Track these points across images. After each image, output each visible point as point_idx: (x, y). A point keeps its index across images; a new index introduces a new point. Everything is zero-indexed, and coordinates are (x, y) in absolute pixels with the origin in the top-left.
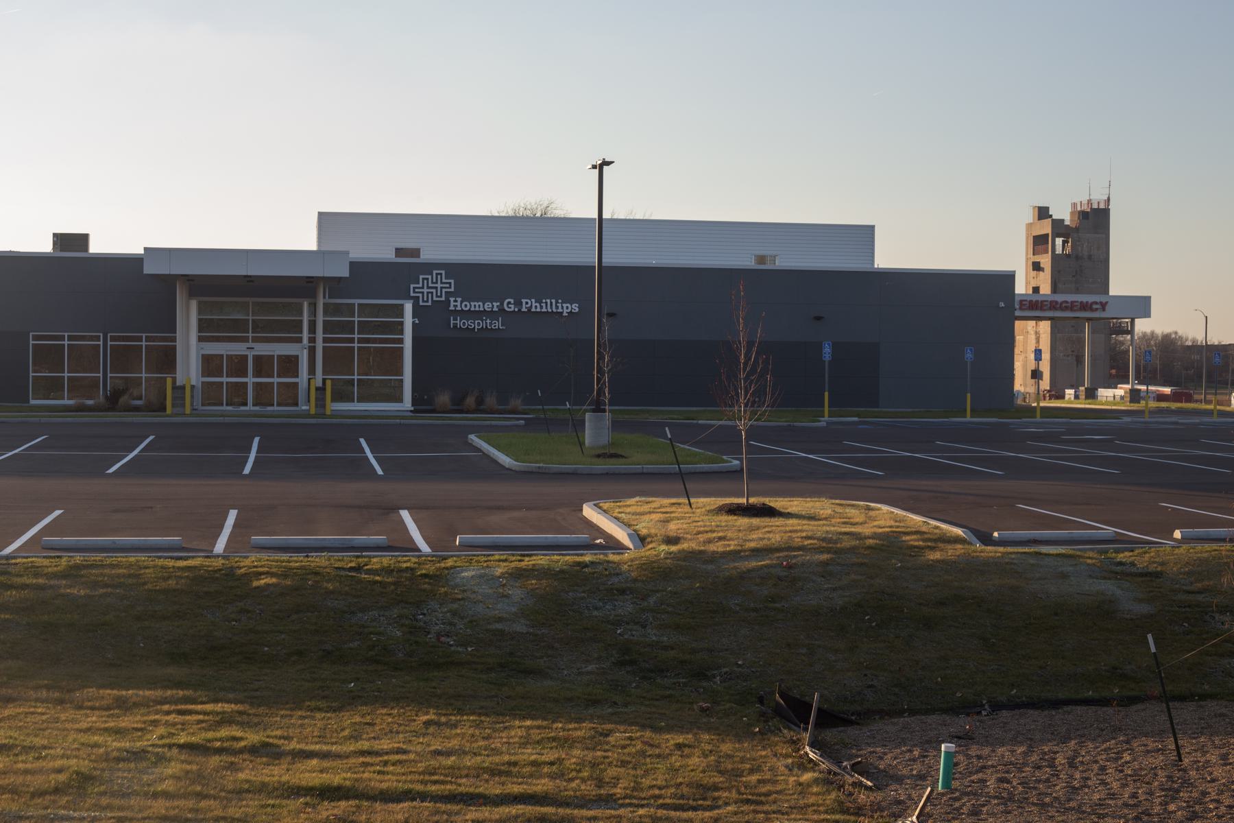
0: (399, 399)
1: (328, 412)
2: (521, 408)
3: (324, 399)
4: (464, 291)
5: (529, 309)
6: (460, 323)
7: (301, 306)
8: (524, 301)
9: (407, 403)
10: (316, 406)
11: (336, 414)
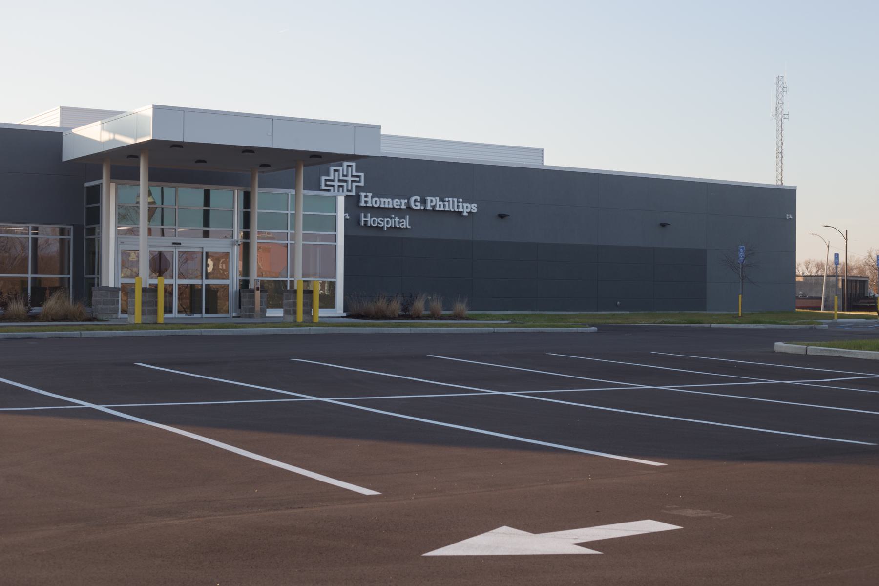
0: (333, 306)
1: (316, 320)
2: (467, 312)
3: (311, 306)
4: (375, 186)
5: (434, 207)
6: (371, 220)
7: (88, 188)
8: (429, 199)
9: (339, 310)
10: (143, 313)
11: (323, 323)
